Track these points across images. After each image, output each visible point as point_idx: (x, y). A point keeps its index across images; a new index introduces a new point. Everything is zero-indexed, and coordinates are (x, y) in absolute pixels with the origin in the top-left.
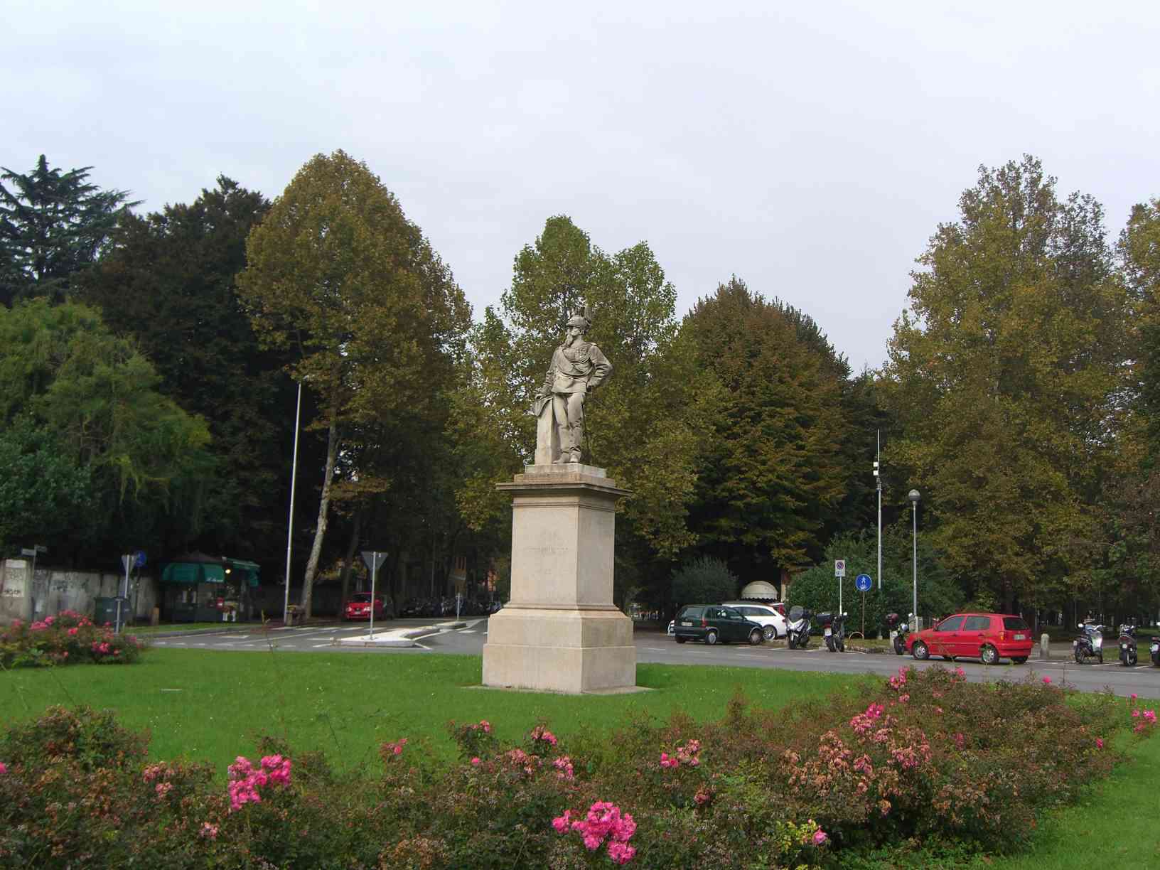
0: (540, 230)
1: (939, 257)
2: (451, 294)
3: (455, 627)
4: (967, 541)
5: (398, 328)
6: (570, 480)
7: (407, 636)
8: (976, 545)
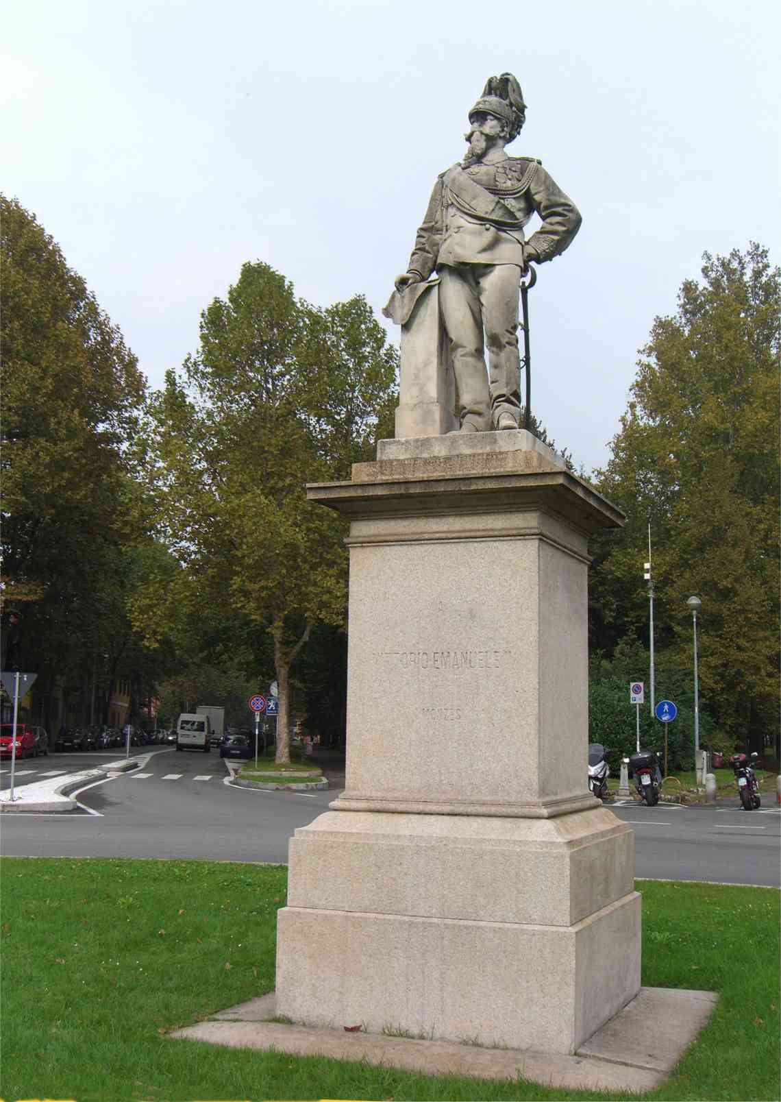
0: (235, 278)
1: (658, 349)
2: (122, 360)
3: (125, 769)
4: (714, 661)
5: (56, 394)
6: (509, 467)
7: (66, 792)
8: (725, 665)
